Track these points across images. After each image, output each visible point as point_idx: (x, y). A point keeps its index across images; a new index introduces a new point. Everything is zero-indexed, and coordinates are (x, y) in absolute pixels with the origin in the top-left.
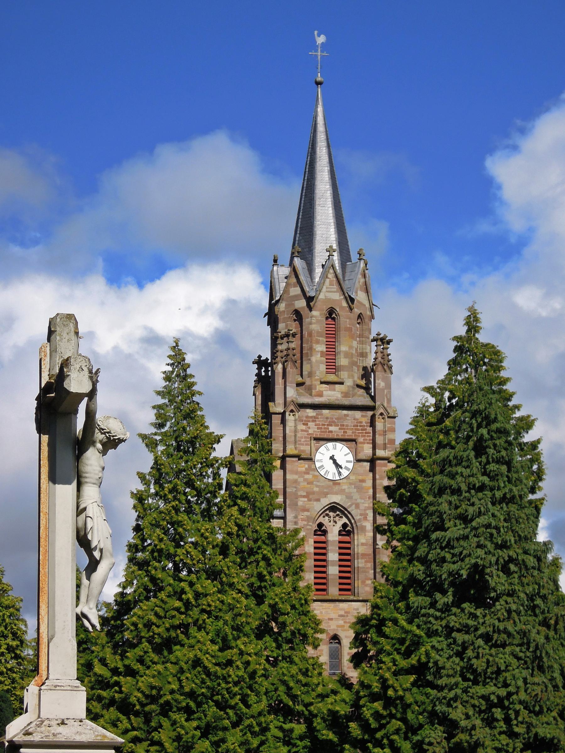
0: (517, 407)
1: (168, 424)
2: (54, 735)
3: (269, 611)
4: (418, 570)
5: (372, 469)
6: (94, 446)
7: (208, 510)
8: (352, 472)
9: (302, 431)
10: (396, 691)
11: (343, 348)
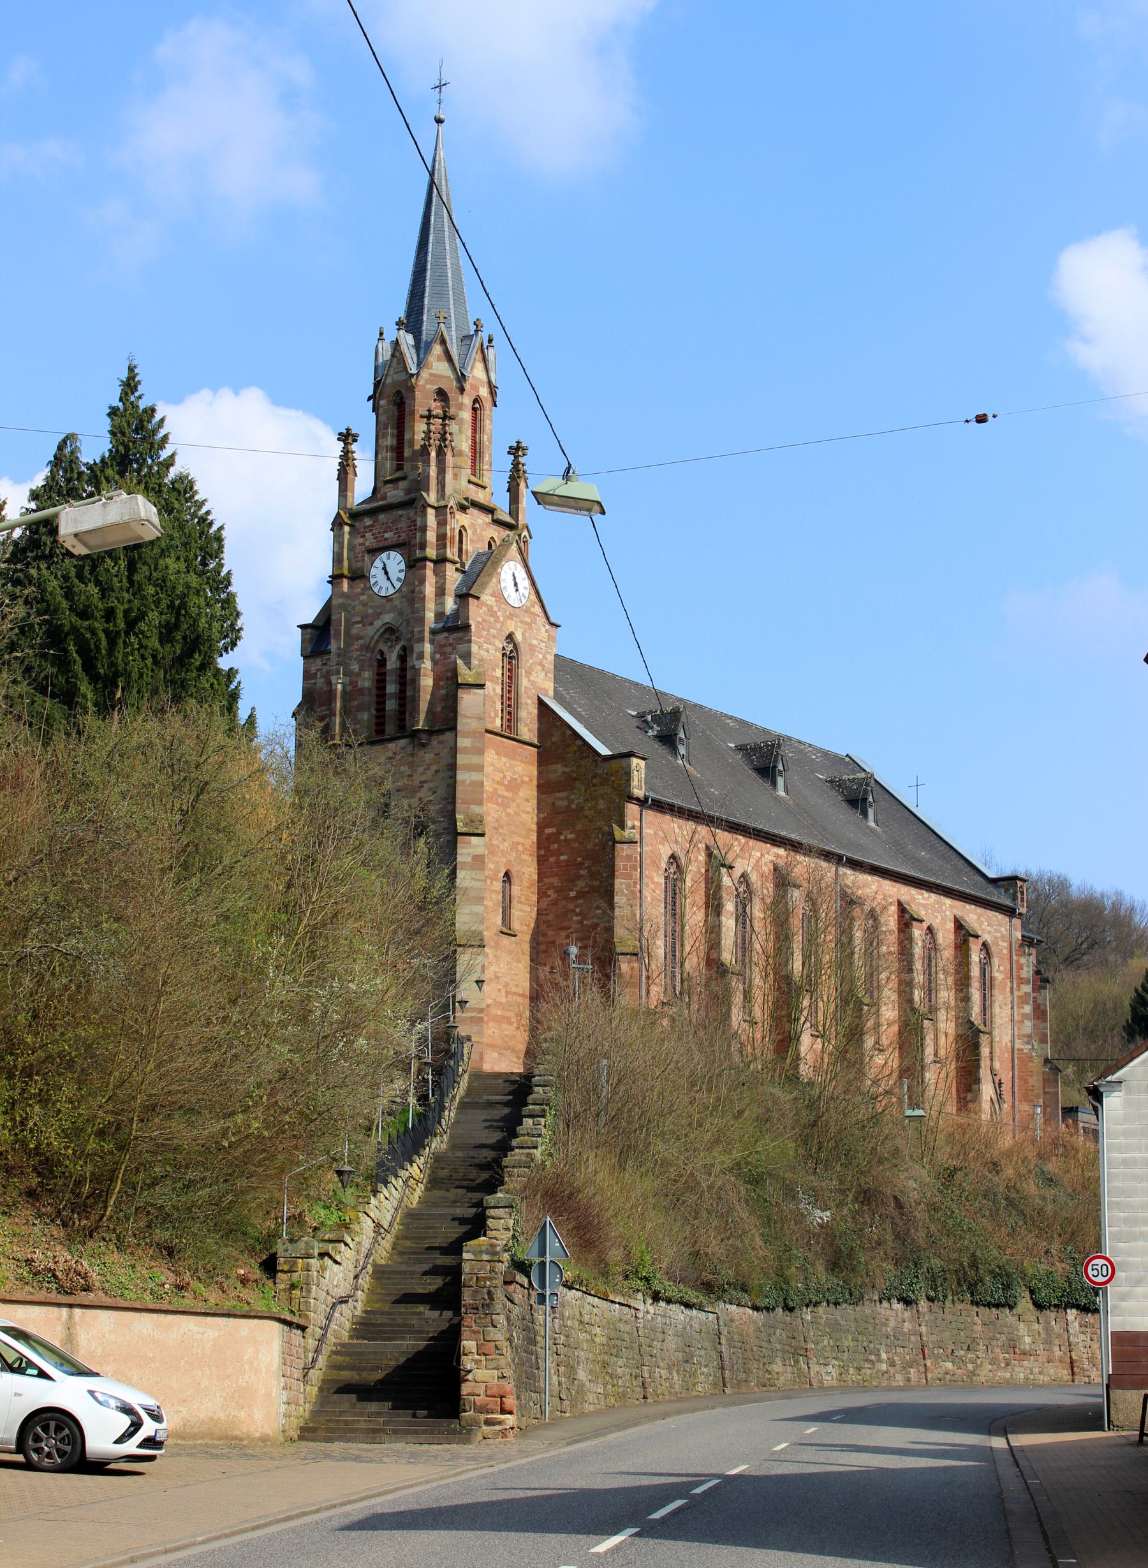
9: (360, 545)
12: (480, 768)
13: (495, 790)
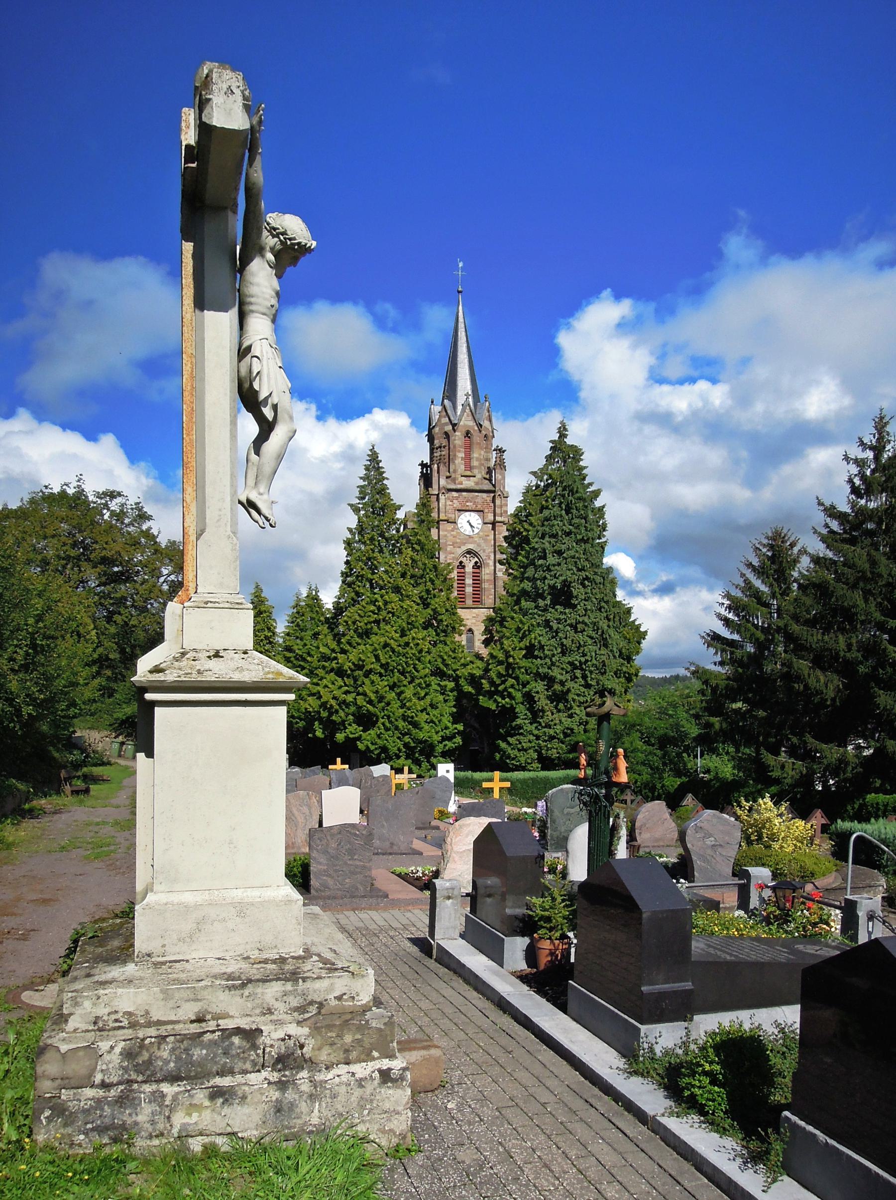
0: (591, 484)
1: (367, 498)
2: (199, 672)
3: (432, 613)
4: (527, 585)
5: (494, 529)
6: (263, 256)
7: (393, 550)
8: (481, 530)
10: (514, 659)
11: (475, 455)
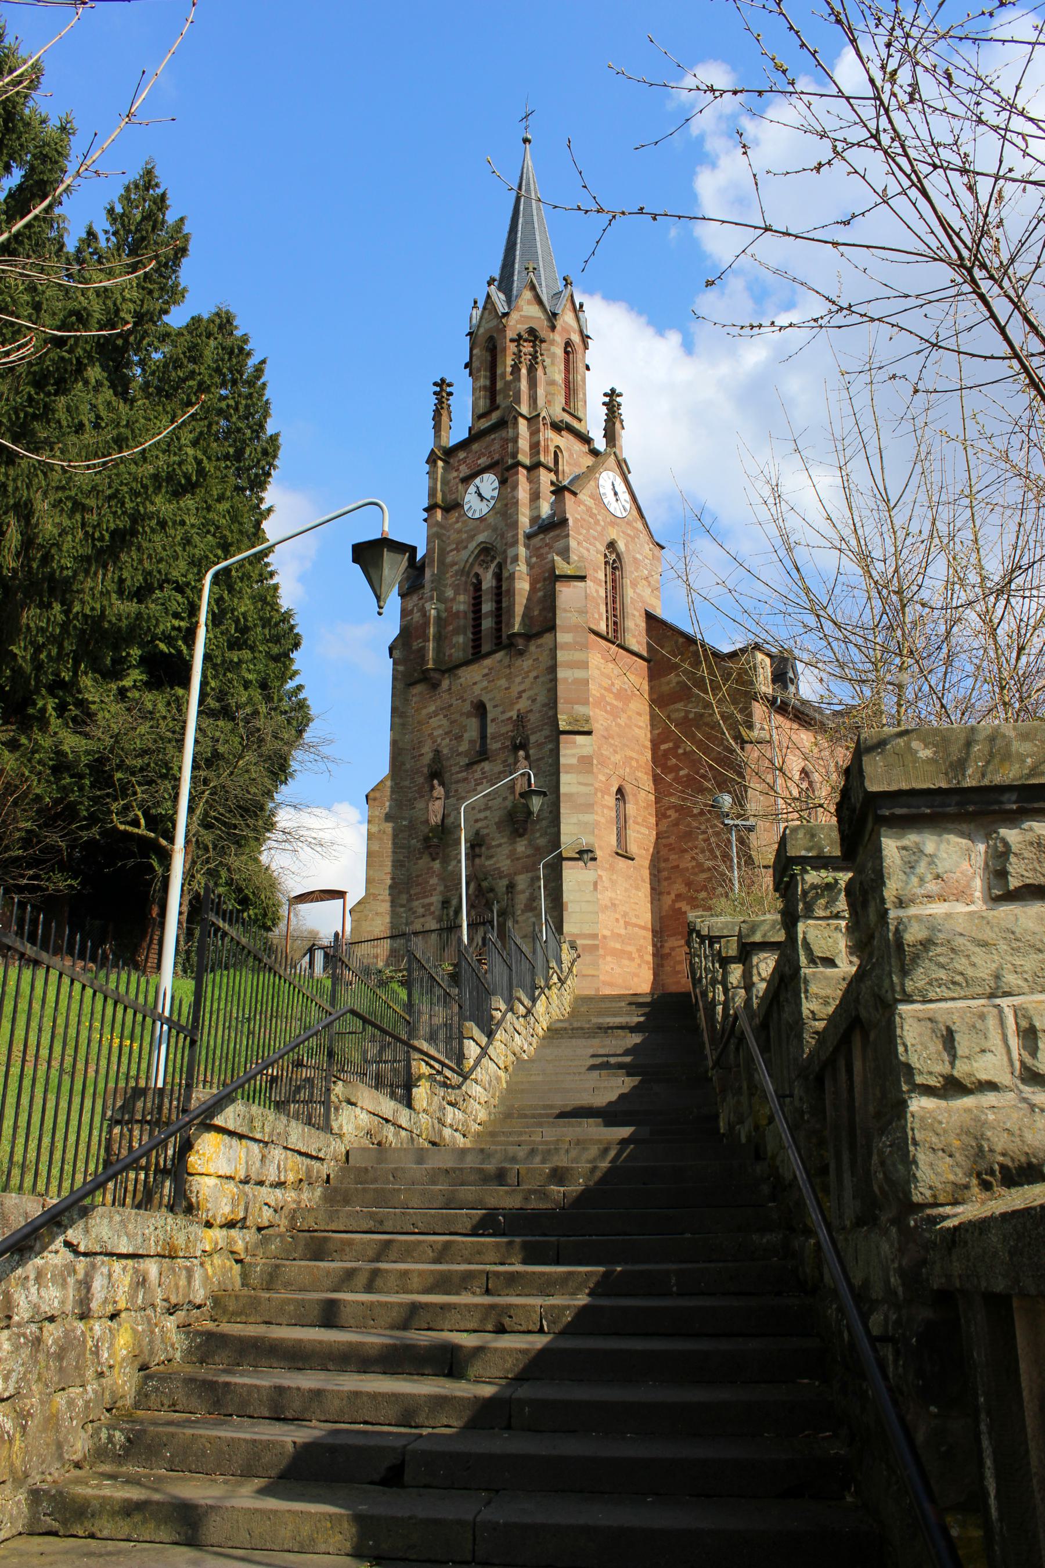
12: (584, 665)
13: (603, 697)
